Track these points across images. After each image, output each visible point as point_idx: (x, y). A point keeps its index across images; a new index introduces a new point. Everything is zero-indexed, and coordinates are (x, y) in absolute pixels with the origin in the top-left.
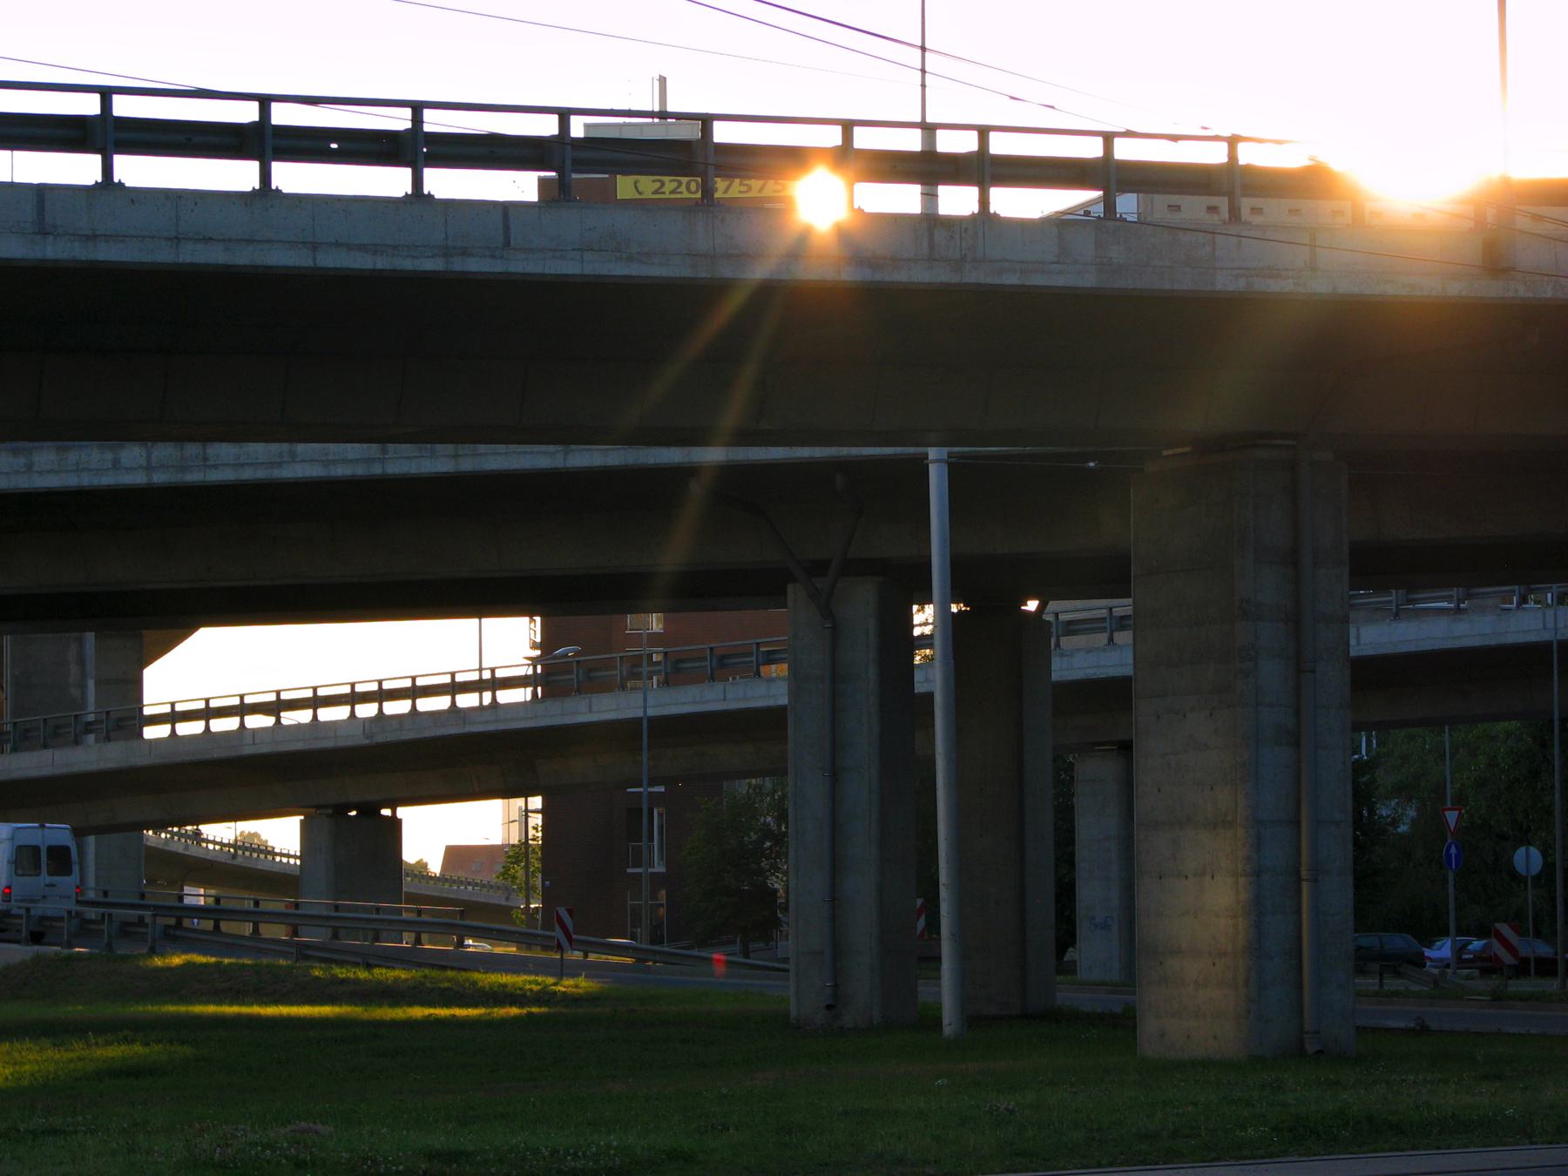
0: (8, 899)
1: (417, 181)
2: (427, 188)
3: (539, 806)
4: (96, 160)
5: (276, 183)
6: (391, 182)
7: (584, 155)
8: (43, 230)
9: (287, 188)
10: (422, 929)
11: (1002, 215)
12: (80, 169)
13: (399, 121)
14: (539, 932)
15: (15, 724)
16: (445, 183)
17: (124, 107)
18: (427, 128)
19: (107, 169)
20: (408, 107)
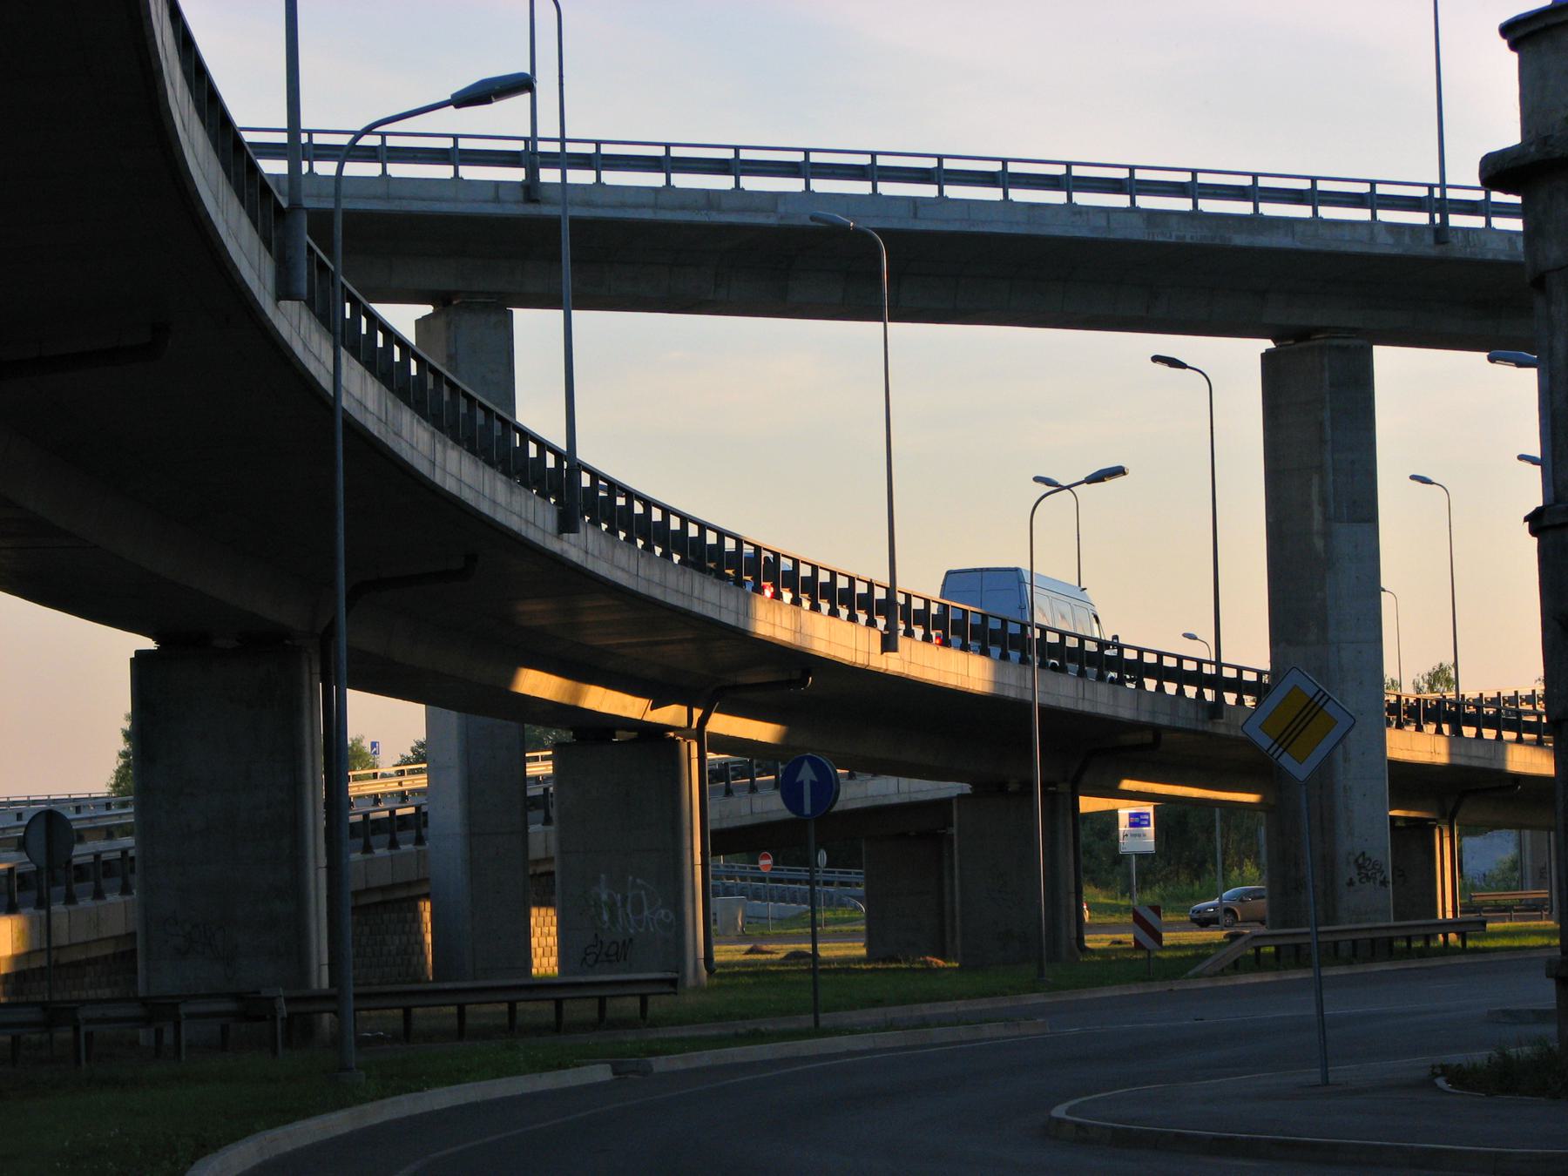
0: (357, 1013)
1: (598, 177)
2: (315, 170)
3: (1195, 689)
4: (663, 176)
5: (673, 182)
6: (656, 180)
7: (318, 152)
8: (497, 199)
9: (466, 177)
10: (1260, 944)
11: (1142, 207)
12: (929, 191)
13: (448, 143)
14: (1392, 923)
15: (946, 607)
16: (887, 189)
17: (745, 155)
18: (878, 164)
19: (737, 182)
20: (1003, 167)
